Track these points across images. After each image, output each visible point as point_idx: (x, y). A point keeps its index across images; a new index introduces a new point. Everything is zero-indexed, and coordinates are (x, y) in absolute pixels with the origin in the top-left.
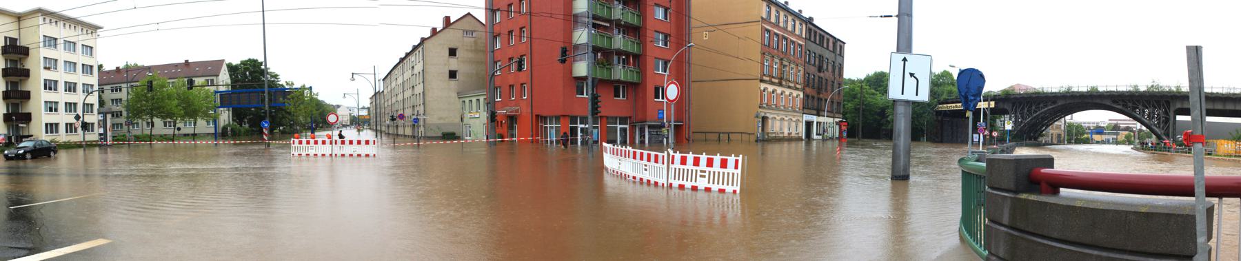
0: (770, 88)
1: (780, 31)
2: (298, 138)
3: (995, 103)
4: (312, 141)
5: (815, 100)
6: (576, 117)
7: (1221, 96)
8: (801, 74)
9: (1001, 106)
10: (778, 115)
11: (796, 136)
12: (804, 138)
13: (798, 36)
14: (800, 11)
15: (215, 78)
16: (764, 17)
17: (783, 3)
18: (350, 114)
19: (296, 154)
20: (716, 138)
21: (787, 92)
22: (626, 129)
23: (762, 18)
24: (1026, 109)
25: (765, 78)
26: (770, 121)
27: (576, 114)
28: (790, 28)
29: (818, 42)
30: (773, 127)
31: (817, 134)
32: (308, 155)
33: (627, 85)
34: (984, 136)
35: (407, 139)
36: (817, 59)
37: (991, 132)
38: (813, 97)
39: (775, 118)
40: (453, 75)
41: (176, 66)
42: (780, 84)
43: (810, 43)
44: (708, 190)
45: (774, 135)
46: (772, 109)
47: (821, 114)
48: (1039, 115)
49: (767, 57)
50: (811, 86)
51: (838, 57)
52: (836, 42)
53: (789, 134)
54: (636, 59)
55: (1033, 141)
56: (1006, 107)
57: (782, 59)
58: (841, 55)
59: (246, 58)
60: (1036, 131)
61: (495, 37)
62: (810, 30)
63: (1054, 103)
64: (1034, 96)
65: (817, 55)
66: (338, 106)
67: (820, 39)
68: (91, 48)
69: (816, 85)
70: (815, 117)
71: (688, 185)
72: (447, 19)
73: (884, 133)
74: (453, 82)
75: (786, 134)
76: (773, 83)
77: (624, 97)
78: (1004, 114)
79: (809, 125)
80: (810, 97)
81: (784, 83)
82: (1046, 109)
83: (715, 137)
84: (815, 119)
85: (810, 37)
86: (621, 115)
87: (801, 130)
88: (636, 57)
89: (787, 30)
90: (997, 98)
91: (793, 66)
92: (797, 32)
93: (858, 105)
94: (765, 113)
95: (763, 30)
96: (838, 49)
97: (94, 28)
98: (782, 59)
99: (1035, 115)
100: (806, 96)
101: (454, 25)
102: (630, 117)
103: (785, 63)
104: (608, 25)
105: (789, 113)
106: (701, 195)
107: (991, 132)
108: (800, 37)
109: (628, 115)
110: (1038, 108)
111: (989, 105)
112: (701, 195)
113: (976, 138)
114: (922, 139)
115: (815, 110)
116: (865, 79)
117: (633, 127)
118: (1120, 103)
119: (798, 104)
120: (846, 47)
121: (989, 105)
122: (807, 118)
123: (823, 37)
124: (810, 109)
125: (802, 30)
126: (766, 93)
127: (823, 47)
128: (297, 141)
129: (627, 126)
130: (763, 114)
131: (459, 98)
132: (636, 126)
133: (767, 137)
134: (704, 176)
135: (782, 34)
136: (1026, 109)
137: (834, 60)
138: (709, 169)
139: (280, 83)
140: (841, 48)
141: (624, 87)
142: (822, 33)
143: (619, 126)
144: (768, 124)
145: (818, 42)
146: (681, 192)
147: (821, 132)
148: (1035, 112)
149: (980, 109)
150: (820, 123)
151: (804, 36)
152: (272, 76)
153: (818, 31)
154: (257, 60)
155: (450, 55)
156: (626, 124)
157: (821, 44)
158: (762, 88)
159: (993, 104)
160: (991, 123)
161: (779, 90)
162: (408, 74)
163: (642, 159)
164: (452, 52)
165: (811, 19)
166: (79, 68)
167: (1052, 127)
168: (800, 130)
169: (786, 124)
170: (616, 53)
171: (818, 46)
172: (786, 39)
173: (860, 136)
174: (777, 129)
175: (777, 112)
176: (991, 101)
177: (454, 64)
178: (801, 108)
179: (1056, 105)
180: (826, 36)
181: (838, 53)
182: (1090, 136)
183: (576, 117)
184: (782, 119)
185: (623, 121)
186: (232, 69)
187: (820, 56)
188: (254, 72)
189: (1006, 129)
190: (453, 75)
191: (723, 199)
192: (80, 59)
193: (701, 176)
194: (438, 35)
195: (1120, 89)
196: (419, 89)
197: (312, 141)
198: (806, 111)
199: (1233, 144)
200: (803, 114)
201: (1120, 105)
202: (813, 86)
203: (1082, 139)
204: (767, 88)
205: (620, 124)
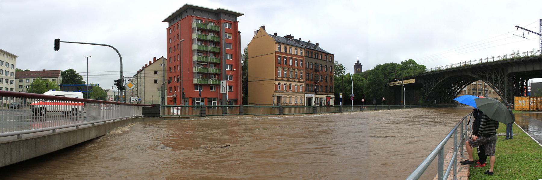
15: (56, 78)
18: (114, 95)
21: (294, 84)
30: (285, 101)
40: (156, 81)
41: (39, 72)
42: (288, 81)
45: (286, 105)
47: (318, 93)
49: (279, 68)
59: (68, 69)
61: (170, 68)
66: (108, 90)
68: (14, 65)
72: (154, 58)
74: (156, 84)
81: (291, 80)
84: (314, 96)
86: (213, 97)
88: (218, 75)
91: (296, 71)
92: (299, 54)
94: (279, 95)
97: (14, 57)
98: (289, 69)
100: (307, 85)
101: (158, 61)
102: (217, 98)
108: (302, 57)
109: (216, 97)
117: (218, 102)
122: (307, 96)
125: (301, 53)
129: (216, 101)
137: (326, 65)
139: (83, 80)
141: (214, 87)
143: (213, 101)
144: (282, 99)
151: (304, 55)
152: (79, 77)
154: (73, 70)
155: (155, 74)
156: (216, 100)
161: (288, 83)
162: (139, 80)
164: (156, 72)
166: (10, 73)
168: (303, 101)
174: (287, 101)
175: (298, 94)
177: (156, 77)
178: (304, 91)
179: (444, 79)
185: (214, 99)
186: (63, 74)
188: (72, 76)
190: (156, 81)
192: (10, 70)
194: (152, 65)
196: (143, 87)
199: (527, 101)
201: (476, 75)
205: (213, 100)
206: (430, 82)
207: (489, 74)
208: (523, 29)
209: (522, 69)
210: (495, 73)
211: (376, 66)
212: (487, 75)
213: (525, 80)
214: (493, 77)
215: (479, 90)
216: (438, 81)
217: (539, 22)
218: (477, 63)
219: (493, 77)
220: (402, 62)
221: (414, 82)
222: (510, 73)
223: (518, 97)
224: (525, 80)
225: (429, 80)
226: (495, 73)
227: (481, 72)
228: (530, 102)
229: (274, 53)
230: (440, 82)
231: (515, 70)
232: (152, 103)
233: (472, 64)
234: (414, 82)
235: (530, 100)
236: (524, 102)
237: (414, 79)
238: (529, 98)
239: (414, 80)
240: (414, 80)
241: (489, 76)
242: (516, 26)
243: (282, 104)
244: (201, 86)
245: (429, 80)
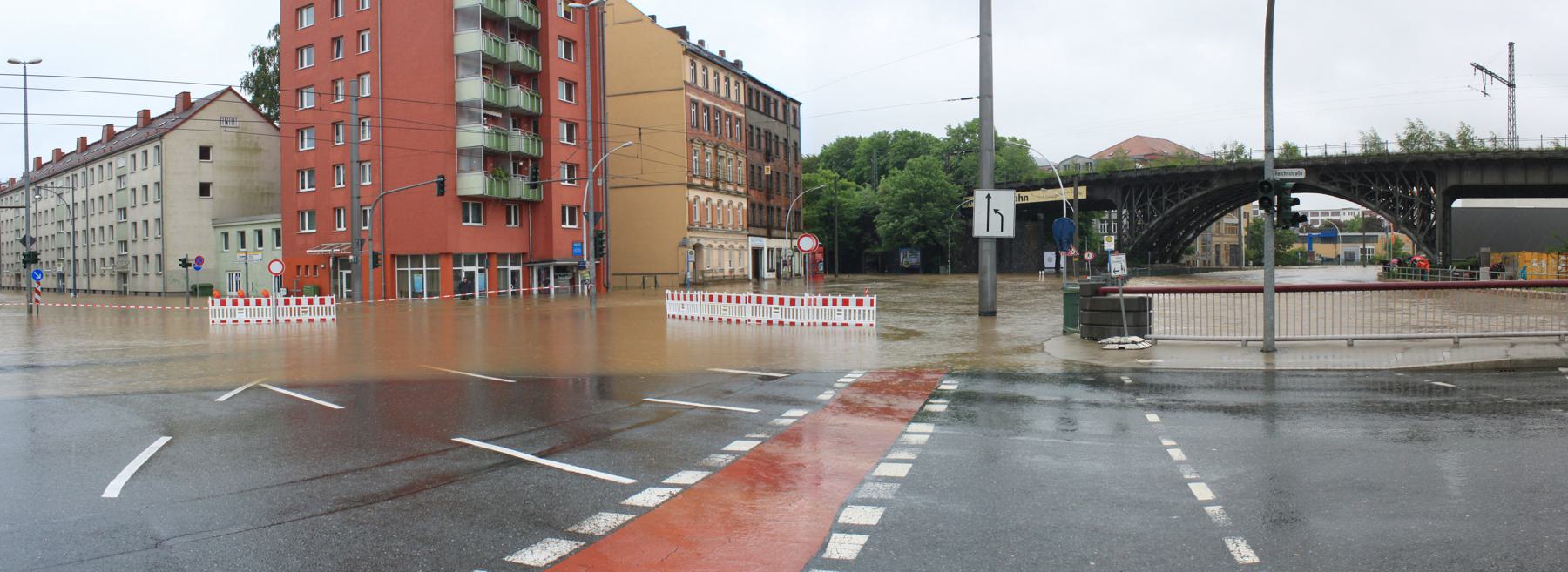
0: (703, 196)
1: (710, 100)
2: (218, 297)
3: (1088, 191)
4: (241, 301)
5: (764, 210)
6: (460, 255)
7: (1538, 155)
8: (742, 169)
9: (1100, 194)
10: (715, 240)
11: (741, 274)
12: (751, 277)
13: (735, 104)
14: (722, 53)
16: (689, 79)
17: (717, 54)
19: (218, 320)
20: (639, 283)
21: (726, 199)
22: (518, 271)
23: (686, 83)
24: (1150, 200)
25: (697, 181)
26: (705, 251)
27: (459, 252)
28: (723, 93)
29: (762, 109)
31: (769, 270)
32: (237, 321)
33: (522, 204)
34: (1069, 259)
35: (151, 299)
36: (763, 139)
37: (1082, 251)
38: (761, 206)
39: (711, 246)
42: (716, 189)
43: (752, 112)
44: (781, 323)
46: (707, 231)
48: (1179, 209)
50: (756, 186)
51: (792, 129)
52: (788, 103)
53: (731, 271)
54: (536, 168)
55: (1168, 265)
56: (1110, 197)
57: (716, 147)
58: (797, 127)
60: (1175, 243)
62: (750, 89)
63: (1206, 184)
64: (1165, 173)
65: (762, 133)
67: (765, 102)
69: (764, 185)
70: (765, 240)
71: (765, 319)
73: (868, 260)
74: (206, 203)
75: (727, 273)
76: (707, 189)
77: (516, 223)
78: (1109, 209)
79: (757, 253)
80: (757, 206)
81: (721, 186)
82: (1190, 198)
83: (638, 281)
84: (764, 243)
85: (750, 101)
87: (746, 264)
88: (535, 160)
89: (719, 97)
90: (1092, 179)
91: (731, 155)
92: (733, 98)
93: (824, 210)
94: (698, 239)
95: (688, 103)
96: (792, 116)
98: (716, 147)
99: (1168, 211)
100: (752, 205)
102: (524, 254)
103: (721, 153)
104: (499, 115)
105: (730, 237)
106: (776, 327)
107: (1082, 251)
108: (736, 105)
110: (1174, 198)
111: (1076, 193)
112: (776, 327)
113: (1050, 260)
114: (942, 268)
115: (762, 227)
116: (822, 155)
117: (528, 269)
118: (1335, 180)
119: (742, 221)
120: (803, 110)
121: (1076, 193)
123: (769, 98)
124: (757, 227)
125: (737, 93)
126: (697, 205)
127: (770, 116)
128: (217, 301)
130: (694, 241)
131: (215, 227)
132: (532, 267)
133: (700, 277)
134: (777, 312)
135: (713, 104)
136: (1150, 200)
137: (786, 136)
138: (781, 306)
140: (796, 113)
142: (767, 92)
143: (511, 268)
144: (702, 255)
145: (762, 109)
146: (769, 327)
147: (775, 267)
148: (1168, 204)
149: (1062, 202)
150: (772, 250)
151: (742, 103)
153: (762, 90)
155: (201, 158)
157: (767, 113)
158: (691, 198)
159: (1083, 192)
160: (1080, 227)
161: (715, 198)
163: (679, 299)
164: (205, 153)
165: (738, 64)
167: (1218, 230)
169: (726, 253)
170: (513, 157)
171: (763, 117)
172: (718, 111)
173: (837, 270)
174: (714, 265)
176: (1080, 185)
178: (745, 227)
179: (1209, 190)
180: (773, 96)
181: (792, 123)
182: (1306, 245)
183: (460, 255)
184: (721, 247)
187: (766, 132)
189: (1106, 248)
190: (205, 189)
191: (793, 332)
193: (775, 312)
195: (1331, 152)
197: (241, 301)
198: (752, 231)
199: (1553, 262)
200: (749, 235)
201: (1334, 184)
202: (760, 186)
203: (1288, 256)
204: (699, 197)
205: (512, 265)
211: (834, 140)
218: (1348, 153)
220: (949, 127)
223: (1530, 254)
228: (1558, 264)
229: (682, 89)
232: (772, 282)
233: (1329, 154)
235: (1558, 259)
236: (1544, 265)
238: (1556, 256)
243: (703, 272)
244: (480, 204)
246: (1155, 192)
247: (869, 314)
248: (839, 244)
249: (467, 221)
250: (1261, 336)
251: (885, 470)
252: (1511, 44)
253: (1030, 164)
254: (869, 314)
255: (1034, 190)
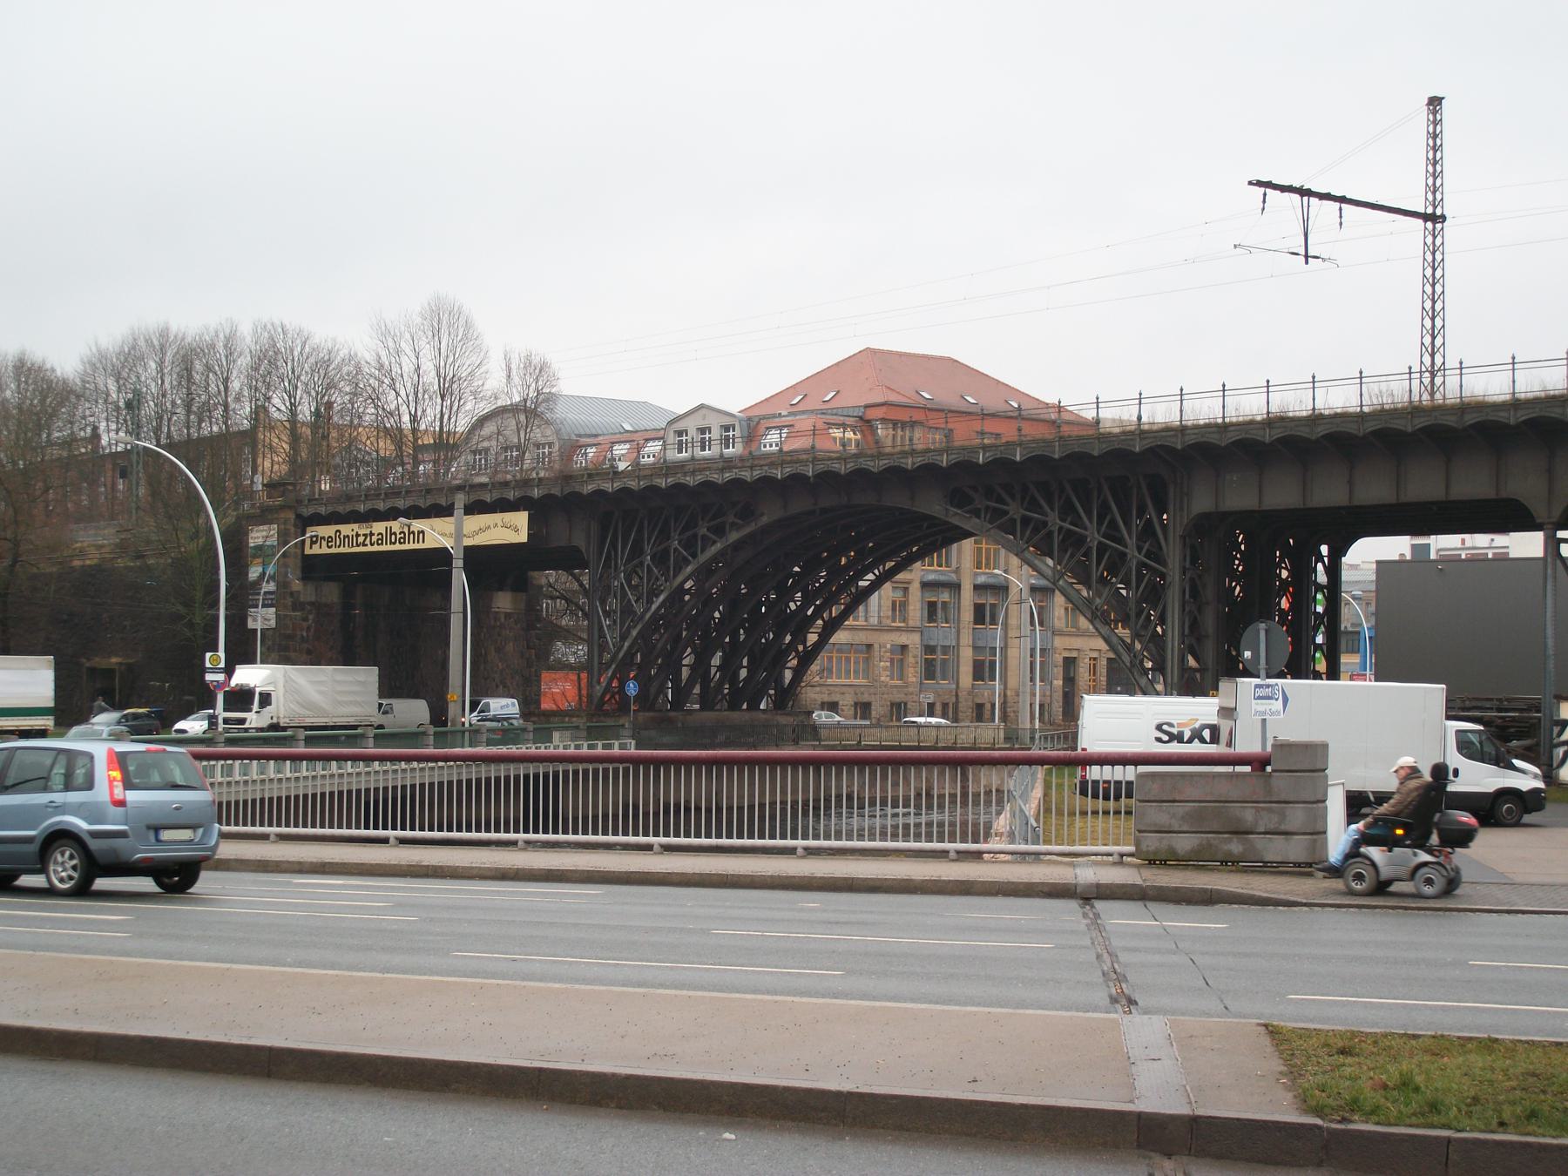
3: (532, 522)
9: (563, 534)
155: (269, 695)
206: (647, 549)
207: (1067, 510)
208: (1304, 192)
209: (1282, 493)
210: (1104, 510)
212: (1054, 520)
213: (1324, 549)
214: (1094, 536)
215: (977, 588)
216: (707, 542)
217: (1422, 115)
219: (1094, 536)
221: (523, 537)
222: (1205, 516)
224: (1324, 549)
225: (640, 531)
226: (1104, 510)
227: (1013, 497)
230: (719, 546)
231: (1240, 495)
234: (523, 537)
237: (525, 514)
239: (521, 519)
240: (521, 519)
241: (1067, 525)
242: (1259, 184)
245: (640, 531)
246: (658, 529)
247: (576, 781)
248: (869, 798)
249: (729, 448)
250: (809, 635)
251: (1238, 588)
252: (1435, 102)
253: (501, 1071)
254: (576, 781)
255: (437, 516)
